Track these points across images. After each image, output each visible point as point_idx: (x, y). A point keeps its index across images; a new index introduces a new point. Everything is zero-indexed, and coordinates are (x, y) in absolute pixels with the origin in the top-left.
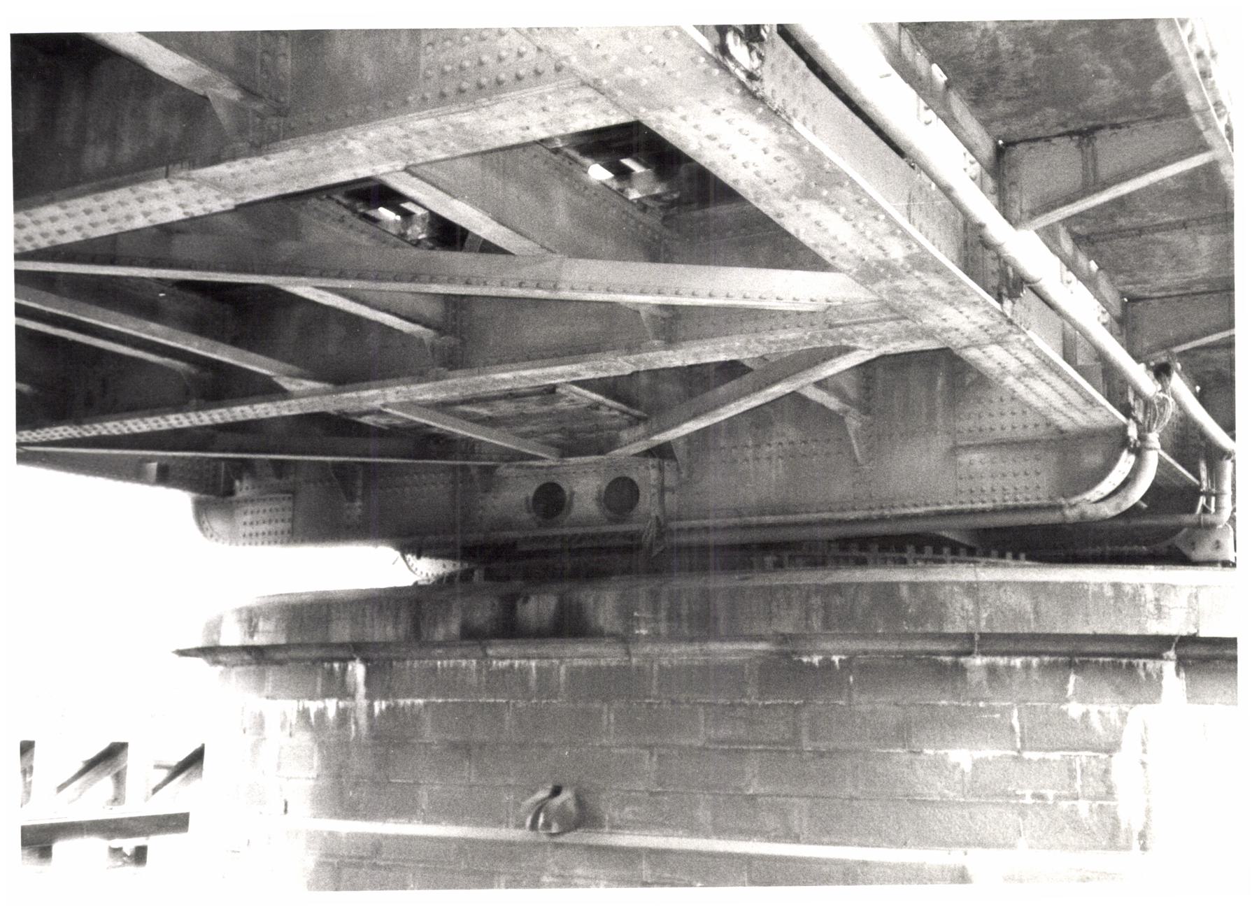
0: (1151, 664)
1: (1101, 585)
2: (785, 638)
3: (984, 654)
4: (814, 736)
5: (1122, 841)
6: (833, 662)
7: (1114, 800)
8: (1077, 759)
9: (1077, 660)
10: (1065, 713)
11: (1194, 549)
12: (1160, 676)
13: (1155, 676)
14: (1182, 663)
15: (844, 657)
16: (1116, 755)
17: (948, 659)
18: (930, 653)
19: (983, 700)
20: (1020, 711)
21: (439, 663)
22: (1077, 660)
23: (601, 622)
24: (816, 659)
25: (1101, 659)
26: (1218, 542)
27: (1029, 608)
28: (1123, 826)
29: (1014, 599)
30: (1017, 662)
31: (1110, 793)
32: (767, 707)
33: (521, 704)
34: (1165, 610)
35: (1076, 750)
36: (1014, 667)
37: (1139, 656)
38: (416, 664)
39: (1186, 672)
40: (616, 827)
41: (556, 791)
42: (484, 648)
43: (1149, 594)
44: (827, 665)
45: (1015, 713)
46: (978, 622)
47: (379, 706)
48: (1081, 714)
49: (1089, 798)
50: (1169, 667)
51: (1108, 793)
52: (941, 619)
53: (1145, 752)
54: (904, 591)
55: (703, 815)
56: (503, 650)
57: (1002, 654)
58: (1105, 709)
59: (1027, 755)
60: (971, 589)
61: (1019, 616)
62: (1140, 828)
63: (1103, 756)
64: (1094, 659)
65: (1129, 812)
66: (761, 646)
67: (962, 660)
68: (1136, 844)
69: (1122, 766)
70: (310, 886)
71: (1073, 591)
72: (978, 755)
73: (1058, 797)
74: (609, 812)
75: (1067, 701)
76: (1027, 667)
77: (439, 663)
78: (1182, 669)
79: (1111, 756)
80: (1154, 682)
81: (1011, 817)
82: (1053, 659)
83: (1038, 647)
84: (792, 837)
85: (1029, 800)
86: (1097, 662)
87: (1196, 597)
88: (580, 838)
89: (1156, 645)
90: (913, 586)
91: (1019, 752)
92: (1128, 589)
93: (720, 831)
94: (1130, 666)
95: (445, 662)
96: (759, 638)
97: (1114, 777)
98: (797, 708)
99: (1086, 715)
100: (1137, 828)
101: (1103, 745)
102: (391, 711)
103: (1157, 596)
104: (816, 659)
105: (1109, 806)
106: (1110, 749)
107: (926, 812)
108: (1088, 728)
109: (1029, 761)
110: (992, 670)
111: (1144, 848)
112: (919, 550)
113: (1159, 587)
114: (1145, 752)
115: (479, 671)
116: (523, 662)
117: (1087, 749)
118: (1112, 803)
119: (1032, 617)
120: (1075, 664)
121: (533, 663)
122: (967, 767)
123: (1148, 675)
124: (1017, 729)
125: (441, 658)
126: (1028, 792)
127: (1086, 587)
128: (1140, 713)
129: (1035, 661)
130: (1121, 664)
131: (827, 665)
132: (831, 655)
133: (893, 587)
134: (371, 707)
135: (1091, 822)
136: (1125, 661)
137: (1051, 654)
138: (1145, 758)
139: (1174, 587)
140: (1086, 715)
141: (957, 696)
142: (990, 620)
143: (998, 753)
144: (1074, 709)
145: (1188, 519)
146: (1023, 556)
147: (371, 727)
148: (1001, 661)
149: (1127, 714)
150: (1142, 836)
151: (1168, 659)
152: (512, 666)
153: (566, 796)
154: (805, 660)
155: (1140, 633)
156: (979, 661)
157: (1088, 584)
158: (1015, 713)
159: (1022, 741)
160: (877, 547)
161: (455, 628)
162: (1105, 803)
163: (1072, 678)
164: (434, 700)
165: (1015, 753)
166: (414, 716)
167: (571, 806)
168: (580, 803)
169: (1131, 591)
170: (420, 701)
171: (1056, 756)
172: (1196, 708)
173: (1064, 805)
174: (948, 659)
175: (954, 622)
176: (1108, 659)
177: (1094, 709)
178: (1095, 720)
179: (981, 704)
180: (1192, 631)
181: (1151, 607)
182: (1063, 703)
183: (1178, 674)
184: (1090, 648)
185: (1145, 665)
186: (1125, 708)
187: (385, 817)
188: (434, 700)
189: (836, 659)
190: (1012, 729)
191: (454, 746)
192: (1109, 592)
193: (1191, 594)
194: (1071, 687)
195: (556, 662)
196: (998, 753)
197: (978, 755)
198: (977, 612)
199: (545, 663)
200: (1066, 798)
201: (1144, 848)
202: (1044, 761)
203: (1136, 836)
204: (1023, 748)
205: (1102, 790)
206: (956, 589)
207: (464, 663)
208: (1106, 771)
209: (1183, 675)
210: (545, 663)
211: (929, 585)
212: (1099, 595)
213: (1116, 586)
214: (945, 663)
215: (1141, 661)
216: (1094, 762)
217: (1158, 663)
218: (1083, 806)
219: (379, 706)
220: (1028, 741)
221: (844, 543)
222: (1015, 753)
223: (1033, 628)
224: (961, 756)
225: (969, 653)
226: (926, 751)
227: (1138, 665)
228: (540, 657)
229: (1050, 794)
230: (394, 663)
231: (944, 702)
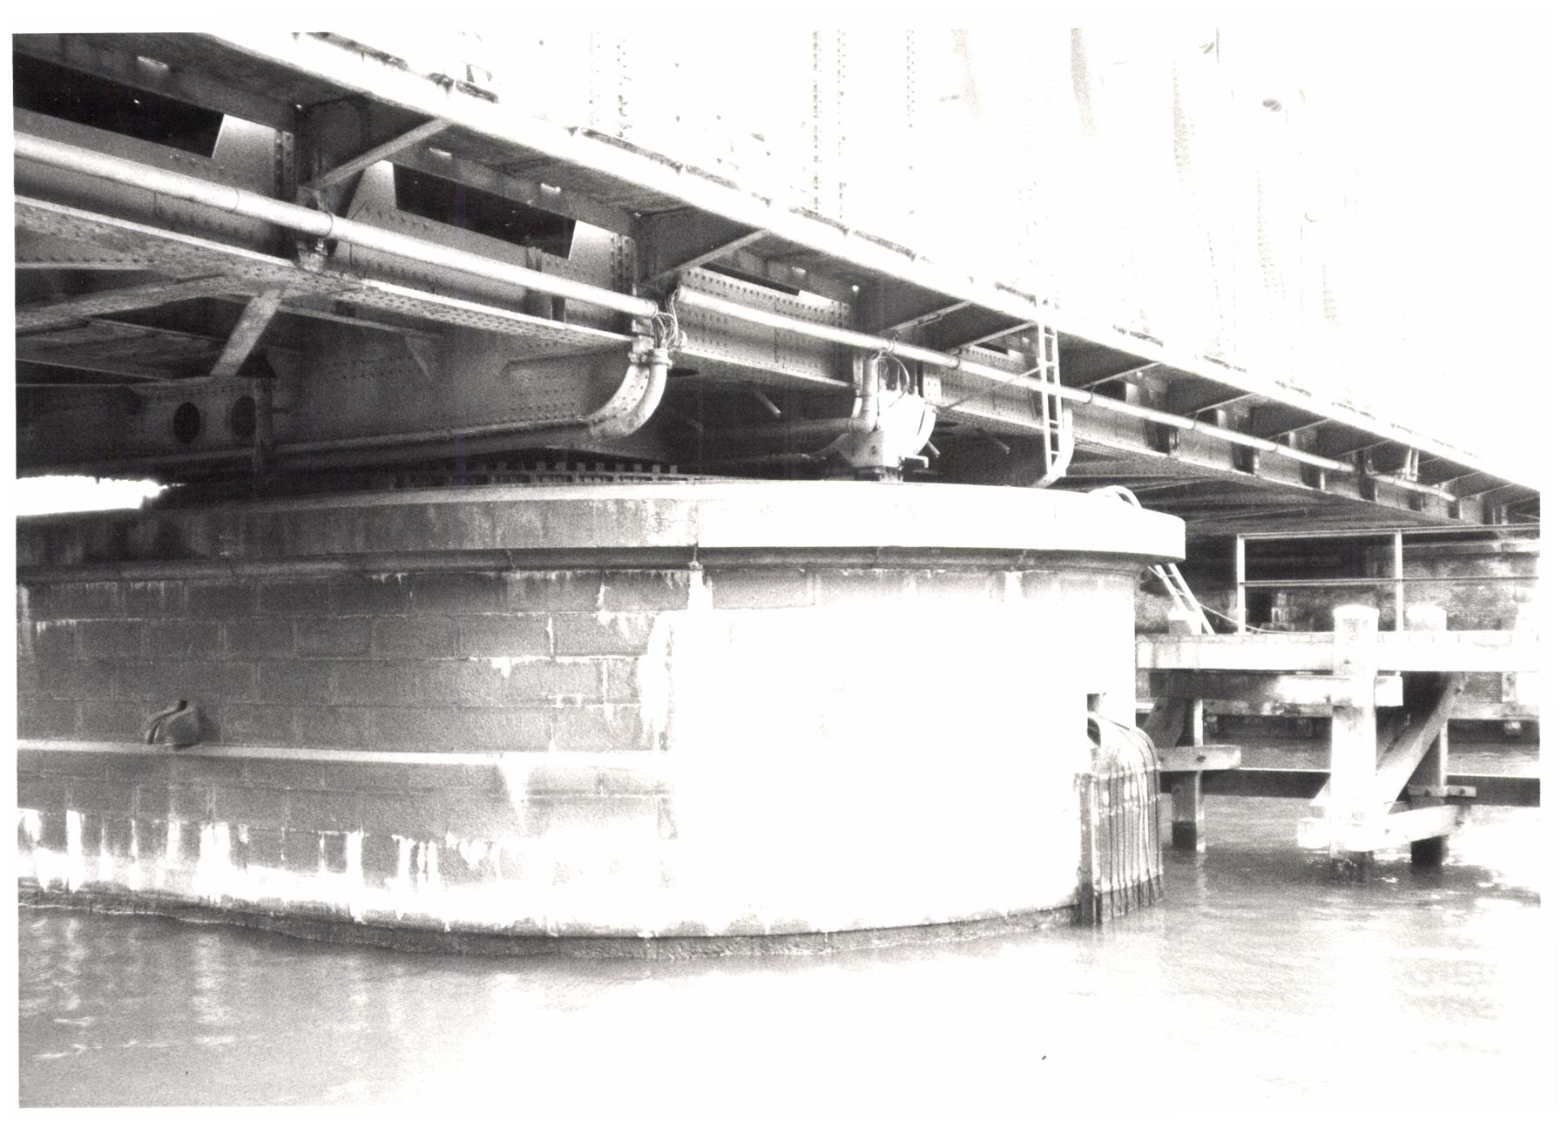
0: (678, 574)
1: (604, 502)
2: (350, 557)
3: (523, 568)
4: (383, 647)
5: (643, 741)
6: (397, 579)
7: (638, 701)
8: (605, 663)
9: (607, 572)
10: (594, 620)
11: (853, 455)
12: (687, 586)
13: (681, 584)
14: (709, 572)
15: (404, 574)
16: (642, 658)
17: (492, 574)
18: (475, 569)
19: (521, 610)
20: (555, 620)
21: (87, 585)
22: (607, 572)
23: (194, 546)
24: (383, 577)
25: (630, 571)
26: (873, 447)
27: (538, 524)
28: (646, 728)
29: (531, 518)
30: (553, 575)
31: (634, 696)
32: (346, 620)
33: (154, 622)
34: (666, 523)
35: (604, 654)
36: (550, 580)
37: (668, 567)
38: (69, 586)
39: (713, 581)
40: (230, 741)
41: (183, 705)
42: (119, 571)
43: (651, 509)
44: (392, 582)
45: (550, 621)
46: (494, 538)
47: (41, 626)
48: (609, 620)
49: (615, 701)
50: (696, 577)
51: (632, 695)
52: (461, 538)
53: (669, 654)
54: (432, 513)
55: (296, 727)
56: (137, 573)
57: (539, 569)
58: (632, 616)
59: (559, 659)
60: (488, 509)
61: (529, 533)
62: (662, 729)
63: (630, 659)
64: (623, 571)
65: (652, 713)
66: (336, 566)
67: (504, 574)
68: (657, 744)
69: (648, 669)
70: (65, 850)
71: (579, 510)
72: (517, 660)
73: (585, 701)
74: (226, 728)
75: (598, 609)
76: (561, 579)
77: (87, 585)
78: (709, 578)
79: (636, 659)
80: (683, 590)
81: (543, 721)
82: (584, 571)
83: (566, 561)
84: (362, 745)
85: (559, 705)
86: (626, 574)
87: (696, 510)
88: (198, 750)
89: (681, 557)
90: (438, 506)
91: (552, 657)
92: (631, 505)
93: (309, 742)
94: (659, 576)
95: (92, 585)
96: (333, 557)
97: (640, 680)
98: (368, 622)
99: (614, 622)
100: (658, 729)
101: (630, 649)
102: (50, 630)
103: (658, 510)
104: (383, 577)
105: (632, 708)
106: (639, 651)
107: (471, 718)
108: (616, 633)
109: (561, 665)
110: (530, 582)
111: (664, 747)
112: (572, 467)
113: (660, 503)
114: (669, 654)
115: (119, 593)
116: (155, 583)
117: (613, 653)
118: (636, 706)
119: (541, 533)
120: (606, 576)
121: (162, 584)
122: (506, 673)
123: (675, 584)
124: (551, 636)
125: (88, 581)
126: (559, 697)
127: (591, 504)
128: (667, 620)
129: (569, 574)
130: (649, 575)
131: (392, 582)
132: (396, 572)
133: (423, 508)
134: (34, 627)
135: (615, 724)
136: (653, 572)
137: (583, 567)
138: (670, 660)
139: (675, 501)
140: (614, 622)
141: (498, 606)
142: (504, 536)
143: (534, 658)
144: (604, 617)
145: (839, 423)
146: (674, 468)
147: (36, 647)
148: (538, 575)
149: (653, 620)
150: (663, 737)
151: (694, 569)
152: (145, 588)
153: (190, 709)
154: (374, 577)
155: (640, 545)
156: (518, 575)
157: (593, 501)
158: (550, 621)
159: (555, 644)
160: (505, 464)
161: (79, 552)
162: (629, 705)
163: (603, 589)
164: (83, 620)
165: (549, 659)
166: (69, 632)
167: (193, 720)
168: (202, 718)
169: (633, 507)
170: (72, 622)
171: (585, 660)
172: (1449, 632)
173: (591, 707)
174: (492, 574)
175: (472, 540)
176: (638, 571)
177: (622, 616)
178: (623, 626)
179: (520, 614)
180: (692, 542)
181: (652, 521)
182: (593, 612)
183: (705, 582)
184: (621, 561)
185: (673, 575)
186: (651, 614)
187: (46, 737)
188: (62, 622)
189: (399, 576)
190: (547, 634)
191: (102, 662)
192: (612, 508)
193: (691, 509)
194: (601, 596)
195: (180, 583)
196: (534, 658)
197: (517, 660)
198: (494, 529)
199: (172, 585)
200: (593, 702)
201: (664, 747)
202: (575, 664)
203: (657, 737)
204: (556, 654)
205: (627, 692)
206: (475, 510)
207: (107, 585)
208: (632, 673)
209: (710, 583)
210: (172, 585)
211: (454, 507)
212: (603, 512)
213: (620, 503)
214: (490, 577)
215: (669, 572)
216: (620, 665)
217: (685, 573)
218: (608, 708)
219: (41, 626)
220: (561, 647)
221: (474, 461)
222: (549, 659)
223: (544, 544)
224: (502, 663)
225: (509, 569)
226: (472, 658)
227: (666, 575)
228: (169, 579)
229: (579, 697)
230: (52, 587)
231: (489, 614)
